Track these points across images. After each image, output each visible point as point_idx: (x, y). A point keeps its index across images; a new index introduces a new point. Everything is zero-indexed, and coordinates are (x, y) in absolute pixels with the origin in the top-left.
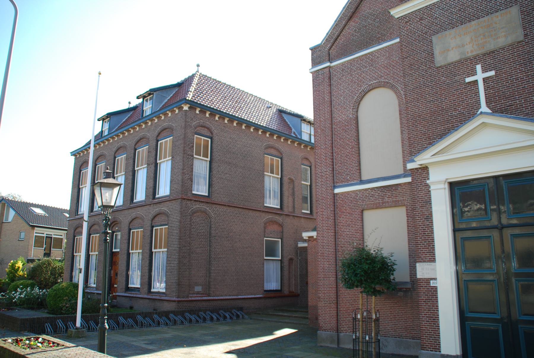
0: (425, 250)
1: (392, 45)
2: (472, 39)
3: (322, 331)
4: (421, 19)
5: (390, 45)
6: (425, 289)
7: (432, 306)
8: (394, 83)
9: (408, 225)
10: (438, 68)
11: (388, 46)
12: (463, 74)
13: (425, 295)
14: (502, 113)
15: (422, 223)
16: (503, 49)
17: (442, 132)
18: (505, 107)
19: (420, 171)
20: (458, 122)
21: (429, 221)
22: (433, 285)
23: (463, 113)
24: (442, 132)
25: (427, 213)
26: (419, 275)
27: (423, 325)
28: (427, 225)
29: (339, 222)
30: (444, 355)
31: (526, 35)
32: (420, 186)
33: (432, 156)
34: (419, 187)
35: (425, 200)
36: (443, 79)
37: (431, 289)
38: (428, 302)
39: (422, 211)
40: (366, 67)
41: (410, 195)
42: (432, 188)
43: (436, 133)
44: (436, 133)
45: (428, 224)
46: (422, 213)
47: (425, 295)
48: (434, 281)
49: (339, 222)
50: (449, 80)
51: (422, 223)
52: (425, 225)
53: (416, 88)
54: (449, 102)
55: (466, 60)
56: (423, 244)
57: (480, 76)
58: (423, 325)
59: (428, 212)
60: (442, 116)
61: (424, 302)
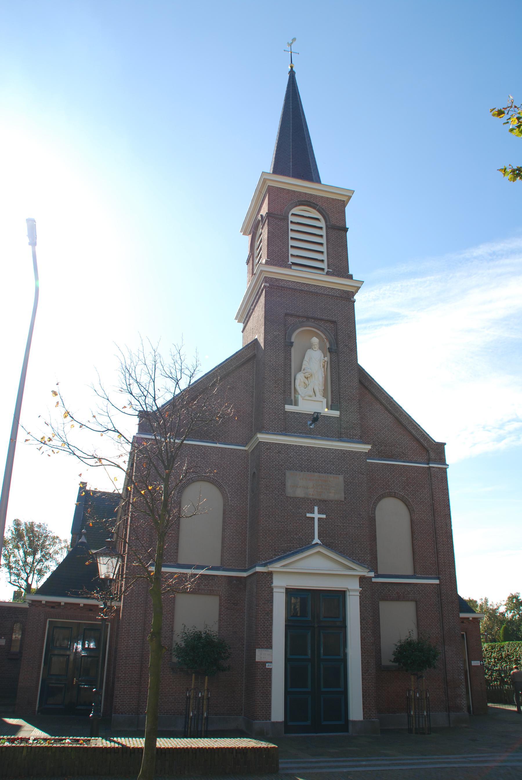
0: (263, 639)
1: (226, 448)
2: (313, 485)
3: (118, 714)
4: (279, 452)
5: (224, 448)
6: (261, 670)
7: (266, 684)
8: (222, 483)
9: (219, 613)
10: (287, 497)
11: (222, 448)
12: (305, 509)
13: (261, 675)
14: (327, 546)
15: (263, 617)
16: (332, 501)
17: (285, 548)
18: (328, 543)
19: (265, 575)
20: (297, 544)
21: (268, 616)
22: (268, 667)
23: (302, 538)
24: (285, 548)
25: (268, 610)
26: (258, 659)
27: (257, 700)
28: (267, 619)
29: (149, 601)
30: (274, 722)
31: (345, 498)
32: (264, 587)
33: (281, 566)
34: (263, 587)
35: (267, 599)
36: (290, 507)
37: (266, 670)
38: (263, 680)
39: (264, 607)
40: (197, 457)
41: (225, 587)
42: (275, 590)
43: (280, 548)
44: (280, 548)
45: (268, 618)
46: (264, 609)
47: (261, 675)
48: (269, 664)
49: (149, 601)
50: (294, 510)
51: (263, 617)
52: (265, 619)
53: (269, 507)
54: (293, 527)
55: (308, 499)
56: (262, 634)
57: (316, 515)
58: (257, 700)
59: (268, 609)
60: (287, 536)
61: (259, 680)
